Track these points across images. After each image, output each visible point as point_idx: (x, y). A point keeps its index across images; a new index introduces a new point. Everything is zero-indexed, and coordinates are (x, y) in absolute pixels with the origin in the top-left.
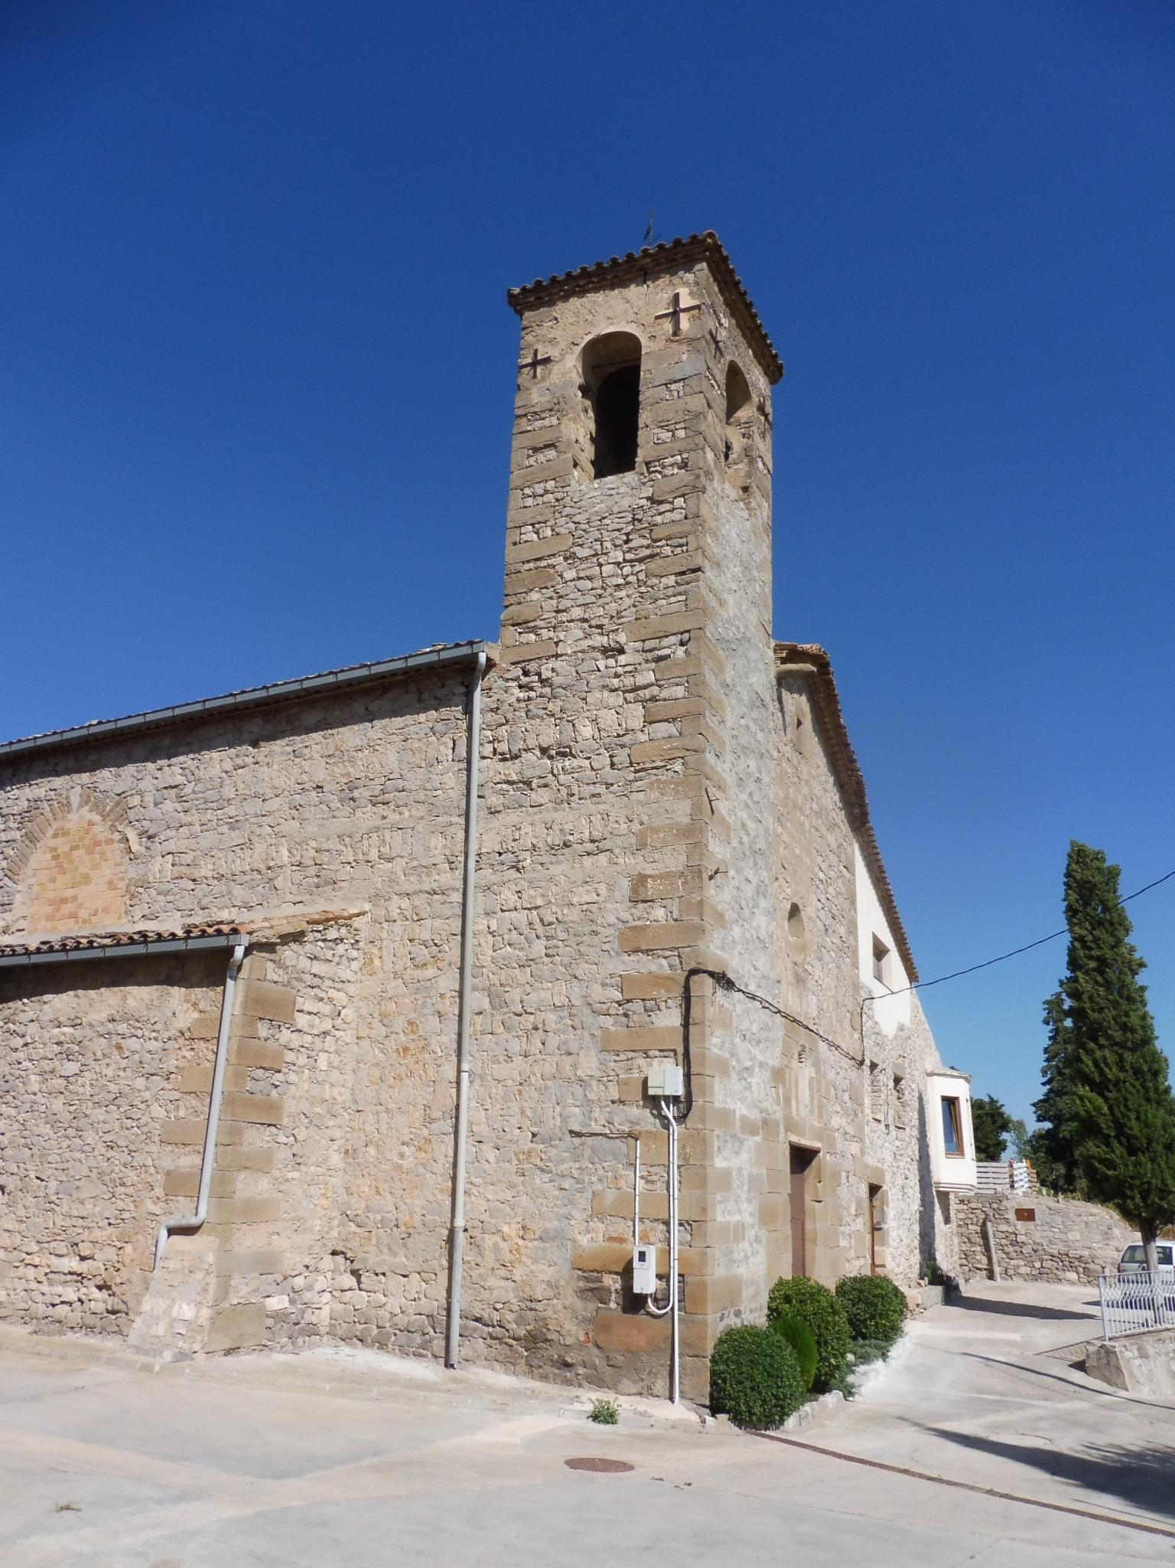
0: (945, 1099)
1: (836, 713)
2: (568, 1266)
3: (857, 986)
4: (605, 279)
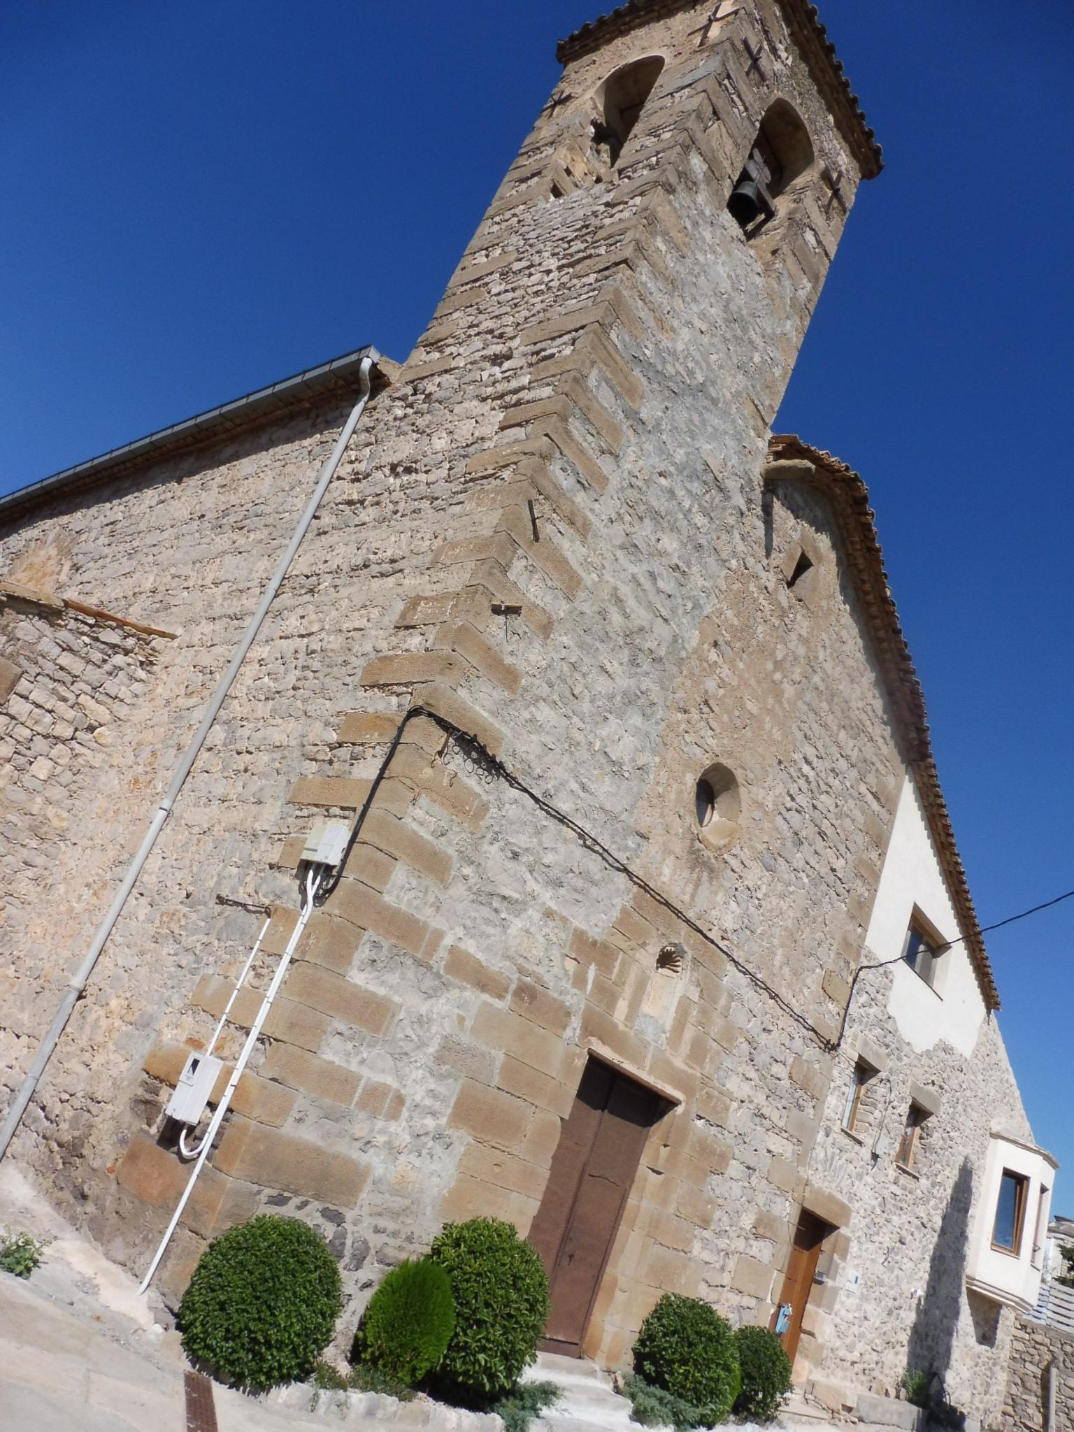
0: (1008, 1173)
1: (879, 580)
2: (140, 1065)
3: (852, 948)
4: (653, 11)
